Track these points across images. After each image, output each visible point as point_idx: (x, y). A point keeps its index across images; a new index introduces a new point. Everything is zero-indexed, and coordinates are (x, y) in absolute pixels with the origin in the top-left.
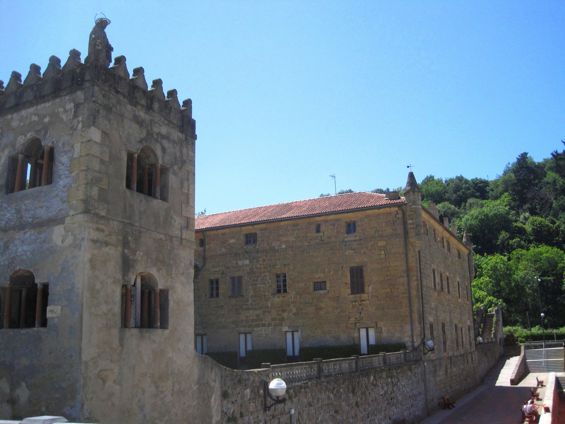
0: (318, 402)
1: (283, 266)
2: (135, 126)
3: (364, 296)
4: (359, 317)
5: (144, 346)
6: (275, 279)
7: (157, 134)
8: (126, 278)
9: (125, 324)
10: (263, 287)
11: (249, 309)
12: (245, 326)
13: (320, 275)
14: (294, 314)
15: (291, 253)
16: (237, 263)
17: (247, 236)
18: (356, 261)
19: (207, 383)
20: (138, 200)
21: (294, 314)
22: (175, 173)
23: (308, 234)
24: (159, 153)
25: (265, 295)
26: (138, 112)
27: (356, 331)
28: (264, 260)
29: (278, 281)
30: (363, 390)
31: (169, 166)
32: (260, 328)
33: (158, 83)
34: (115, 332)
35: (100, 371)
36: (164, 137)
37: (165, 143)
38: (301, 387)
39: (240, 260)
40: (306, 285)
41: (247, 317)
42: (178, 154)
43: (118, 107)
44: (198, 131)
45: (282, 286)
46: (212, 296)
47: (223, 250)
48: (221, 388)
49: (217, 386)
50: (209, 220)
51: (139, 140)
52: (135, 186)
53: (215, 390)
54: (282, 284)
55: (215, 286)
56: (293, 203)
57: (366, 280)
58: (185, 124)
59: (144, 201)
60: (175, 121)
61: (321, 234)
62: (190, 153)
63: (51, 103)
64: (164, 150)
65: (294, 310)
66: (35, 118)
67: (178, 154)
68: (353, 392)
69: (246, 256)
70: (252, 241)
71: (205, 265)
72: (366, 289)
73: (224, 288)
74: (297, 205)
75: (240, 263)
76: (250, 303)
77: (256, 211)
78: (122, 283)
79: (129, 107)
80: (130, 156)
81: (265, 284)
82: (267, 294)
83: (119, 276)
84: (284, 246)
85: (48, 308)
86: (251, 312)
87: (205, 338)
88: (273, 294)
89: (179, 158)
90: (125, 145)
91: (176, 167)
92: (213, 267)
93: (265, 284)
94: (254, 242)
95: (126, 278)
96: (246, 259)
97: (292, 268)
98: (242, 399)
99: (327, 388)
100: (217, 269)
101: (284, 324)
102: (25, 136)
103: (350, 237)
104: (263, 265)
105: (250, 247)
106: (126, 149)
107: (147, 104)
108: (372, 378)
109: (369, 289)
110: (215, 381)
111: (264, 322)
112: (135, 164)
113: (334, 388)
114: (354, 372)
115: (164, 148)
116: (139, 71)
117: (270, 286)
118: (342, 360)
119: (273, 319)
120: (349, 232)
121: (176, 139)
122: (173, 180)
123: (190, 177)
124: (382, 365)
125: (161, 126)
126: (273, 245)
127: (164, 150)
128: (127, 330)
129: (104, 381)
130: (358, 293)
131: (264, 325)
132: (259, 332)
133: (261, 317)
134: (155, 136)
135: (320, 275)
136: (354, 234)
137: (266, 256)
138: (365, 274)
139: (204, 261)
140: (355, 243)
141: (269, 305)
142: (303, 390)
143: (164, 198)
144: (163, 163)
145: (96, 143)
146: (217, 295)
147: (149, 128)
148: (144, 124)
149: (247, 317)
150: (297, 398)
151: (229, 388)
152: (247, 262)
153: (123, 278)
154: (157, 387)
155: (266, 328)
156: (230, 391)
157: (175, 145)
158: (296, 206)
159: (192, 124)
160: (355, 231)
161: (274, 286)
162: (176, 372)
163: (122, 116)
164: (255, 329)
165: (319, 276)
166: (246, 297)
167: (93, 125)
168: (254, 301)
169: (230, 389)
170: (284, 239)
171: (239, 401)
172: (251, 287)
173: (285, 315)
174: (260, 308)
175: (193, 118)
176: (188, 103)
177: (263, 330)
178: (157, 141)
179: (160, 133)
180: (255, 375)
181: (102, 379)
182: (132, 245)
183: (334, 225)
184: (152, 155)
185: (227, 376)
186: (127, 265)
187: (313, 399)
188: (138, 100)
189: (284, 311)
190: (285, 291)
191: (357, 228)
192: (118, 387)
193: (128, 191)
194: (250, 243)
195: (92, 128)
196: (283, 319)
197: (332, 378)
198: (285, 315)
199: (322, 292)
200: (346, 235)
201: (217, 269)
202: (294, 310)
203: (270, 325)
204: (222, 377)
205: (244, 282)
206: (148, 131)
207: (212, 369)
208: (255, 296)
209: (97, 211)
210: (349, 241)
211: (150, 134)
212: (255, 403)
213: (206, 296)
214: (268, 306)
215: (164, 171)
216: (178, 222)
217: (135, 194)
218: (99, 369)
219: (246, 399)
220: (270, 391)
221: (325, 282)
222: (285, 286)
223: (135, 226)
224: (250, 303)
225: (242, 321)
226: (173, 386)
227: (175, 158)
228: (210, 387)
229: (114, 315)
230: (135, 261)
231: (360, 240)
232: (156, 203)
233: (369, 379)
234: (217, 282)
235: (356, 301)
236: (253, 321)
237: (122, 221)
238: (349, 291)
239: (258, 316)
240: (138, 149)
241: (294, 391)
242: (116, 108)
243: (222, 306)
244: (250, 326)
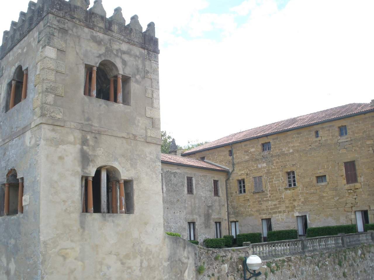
0: (302, 274)
1: (292, 166)
2: (93, 44)
3: (357, 185)
4: (354, 202)
5: (106, 229)
6: (286, 176)
7: (117, 50)
8: (85, 170)
9: (86, 210)
10: (278, 183)
11: (268, 200)
12: (266, 214)
13: (320, 171)
14: (302, 202)
15: (297, 155)
16: (257, 166)
17: (263, 145)
18: (349, 158)
19: (180, 260)
20: (100, 106)
21: (302, 202)
22: (137, 81)
23: (309, 139)
24: (119, 65)
25: (279, 189)
26: (96, 33)
27: (353, 213)
28: (277, 163)
29: (289, 178)
30: (350, 262)
31: (130, 76)
32: (278, 215)
33: (134, 19)
34: (76, 215)
35: (60, 250)
36: (124, 53)
37: (126, 57)
38: (284, 261)
39: (259, 164)
40: (310, 179)
41: (267, 207)
42: (140, 66)
43: (74, 30)
44: (160, 47)
45: (292, 181)
46: (241, 192)
47: (247, 157)
48: (195, 264)
49: (191, 263)
50: (236, 136)
51: (98, 55)
52: (94, 93)
53: (189, 265)
54: (292, 180)
55: (242, 185)
56: (298, 117)
57: (358, 172)
58: (148, 42)
59: (104, 105)
60: (136, 40)
61: (319, 138)
62: (154, 65)
63: (27, 37)
64: (124, 63)
65: (302, 200)
66: (20, 51)
67: (140, 66)
68: (340, 264)
69: (264, 160)
70: (267, 149)
71: (234, 170)
72: (359, 179)
73: (248, 185)
74: (302, 119)
75: (260, 166)
76: (268, 196)
77: (270, 126)
78: (81, 174)
79: (86, 30)
80: (89, 69)
81: (279, 180)
82: (281, 188)
83: (79, 169)
84: (291, 151)
85: (23, 198)
86: (270, 202)
87: (237, 223)
88: (286, 189)
89: (142, 69)
90: (82, 60)
91: (138, 77)
92: (240, 170)
93: (279, 180)
94: (269, 150)
95: (85, 170)
96: (264, 162)
97: (299, 166)
98: (219, 272)
99: (311, 262)
100: (243, 172)
101: (295, 211)
102: (15, 66)
103: (343, 139)
104: (277, 166)
105: (266, 153)
106: (83, 63)
107: (105, 26)
108: (360, 252)
109: (361, 179)
110: (189, 258)
111: (280, 210)
112: (94, 76)
113: (319, 261)
114: (340, 247)
115: (125, 61)
116: (134, 19)
117: (283, 182)
118: (327, 237)
119: (287, 207)
120: (341, 134)
121: (138, 54)
122: (134, 87)
123: (154, 84)
124: (370, 241)
125: (122, 44)
126: (283, 150)
127: (124, 63)
128: (88, 214)
129: (65, 257)
130: (352, 183)
131: (280, 212)
132: (277, 218)
133: (278, 206)
134: (115, 52)
135: (320, 171)
136: (346, 136)
137: (279, 159)
138: (357, 168)
139: (234, 167)
140: (347, 143)
141: (283, 197)
142: (286, 264)
143: (126, 101)
144: (124, 73)
145: (51, 59)
146: (244, 191)
147: (108, 45)
148: (103, 43)
149: (267, 207)
150: (280, 271)
151: (204, 263)
152: (265, 165)
153: (82, 171)
154: (123, 264)
155: (282, 214)
156: (206, 266)
157: (137, 58)
158: (300, 119)
159: (155, 42)
160: (346, 134)
161: (286, 182)
162: (144, 251)
163: (79, 37)
164: (274, 215)
165: (320, 172)
166: (266, 192)
167: (49, 45)
168: (271, 194)
169: (206, 264)
170: (291, 145)
171: (216, 275)
172: (269, 184)
173: (296, 204)
174: (277, 199)
175: (156, 36)
176: (151, 26)
177: (280, 216)
178: (117, 56)
179: (120, 49)
180: (232, 252)
181: (63, 256)
182: (91, 143)
183: (329, 130)
184: (114, 68)
185: (202, 254)
186: (85, 159)
187: (296, 271)
188: (95, 23)
189: (294, 200)
190: (295, 185)
191: (348, 131)
192: (80, 263)
193: (86, 98)
194: (266, 150)
195: (47, 47)
196: (294, 207)
197: (317, 253)
198: (296, 204)
199: (323, 184)
200: (339, 138)
201: (243, 172)
202: (302, 200)
203: (284, 212)
204: (196, 254)
205: (263, 180)
206: (106, 48)
207: (184, 248)
208: (272, 191)
209: (52, 115)
210: (342, 142)
211: (109, 50)
212: (234, 276)
213: (236, 192)
214: (282, 198)
215: (126, 80)
216: (142, 122)
217: (94, 99)
218: (59, 248)
219: (224, 273)
220: (247, 265)
221: (325, 176)
222: (294, 181)
223: (94, 126)
224: (268, 196)
225: (264, 210)
226: (141, 263)
227: (138, 69)
228: (183, 263)
229: (73, 202)
230: (95, 156)
231: (351, 140)
232: (119, 107)
233: (356, 253)
234: (243, 181)
235: (351, 190)
236: (271, 209)
237: (80, 122)
238: (345, 181)
239: (275, 205)
240: (97, 63)
241: (276, 264)
242: (72, 31)
243: (248, 200)
244: (270, 213)
